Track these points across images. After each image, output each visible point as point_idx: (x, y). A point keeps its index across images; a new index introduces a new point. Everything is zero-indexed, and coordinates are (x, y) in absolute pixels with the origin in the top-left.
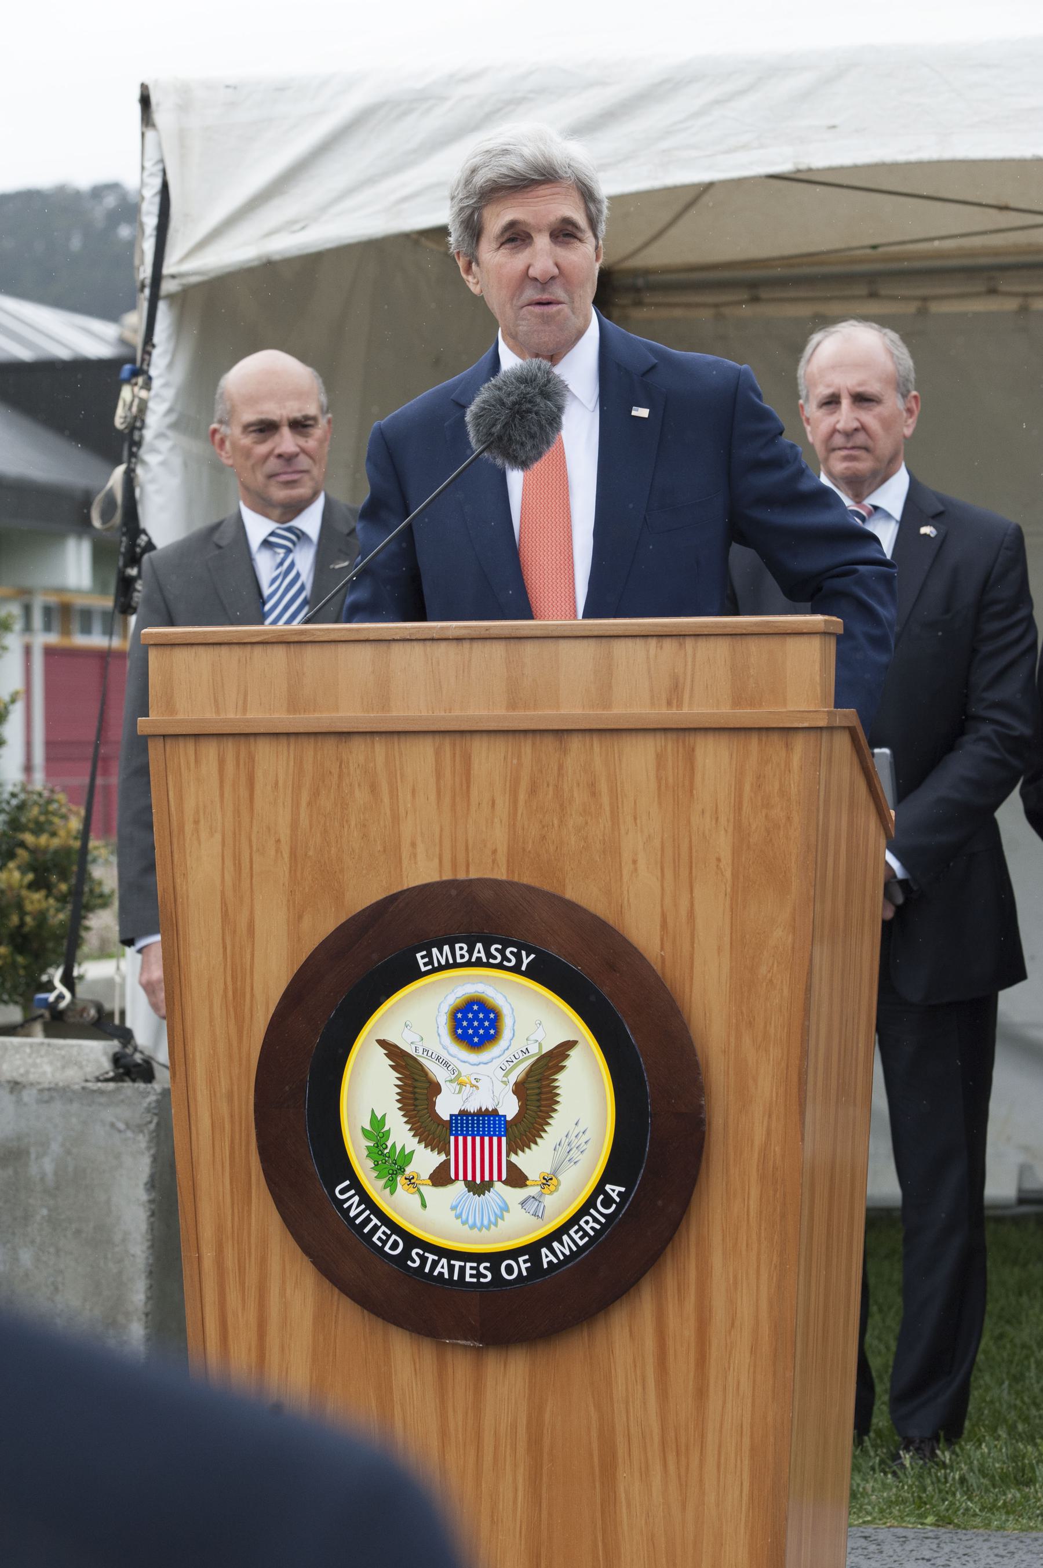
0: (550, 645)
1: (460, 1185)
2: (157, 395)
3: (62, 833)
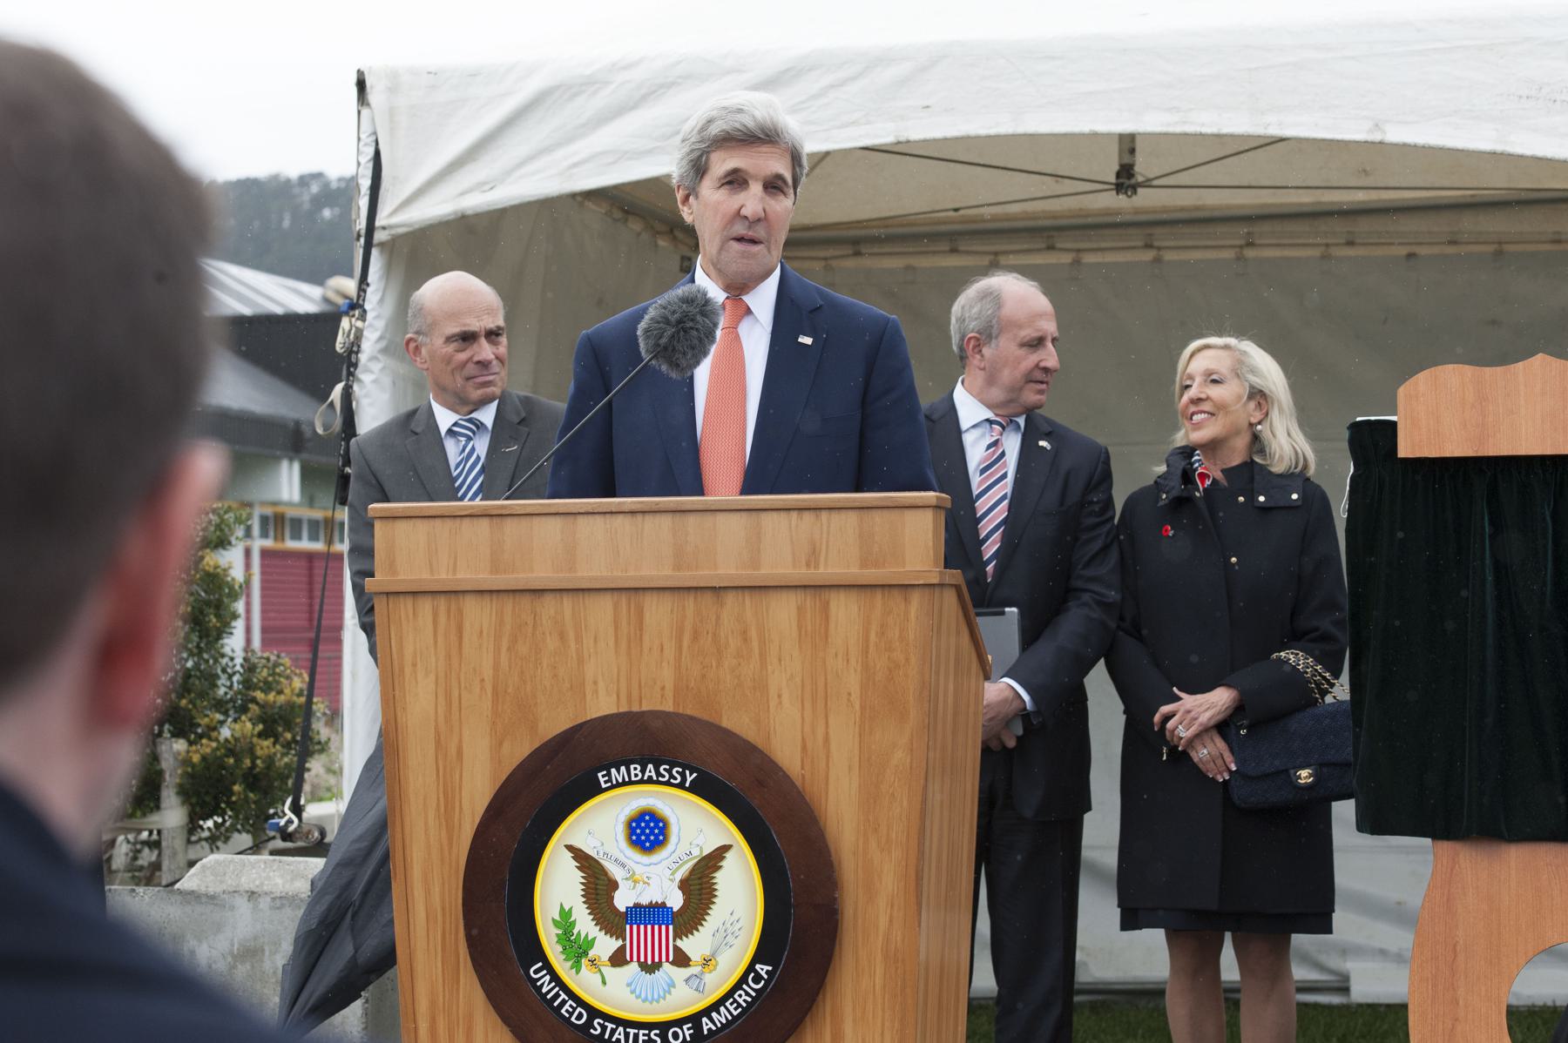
0: (709, 518)
1: (634, 966)
2: (371, 325)
3: (287, 691)
